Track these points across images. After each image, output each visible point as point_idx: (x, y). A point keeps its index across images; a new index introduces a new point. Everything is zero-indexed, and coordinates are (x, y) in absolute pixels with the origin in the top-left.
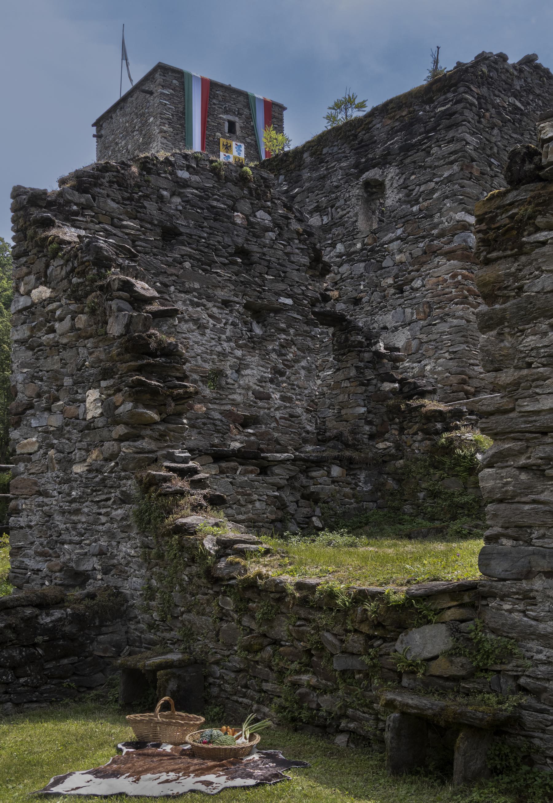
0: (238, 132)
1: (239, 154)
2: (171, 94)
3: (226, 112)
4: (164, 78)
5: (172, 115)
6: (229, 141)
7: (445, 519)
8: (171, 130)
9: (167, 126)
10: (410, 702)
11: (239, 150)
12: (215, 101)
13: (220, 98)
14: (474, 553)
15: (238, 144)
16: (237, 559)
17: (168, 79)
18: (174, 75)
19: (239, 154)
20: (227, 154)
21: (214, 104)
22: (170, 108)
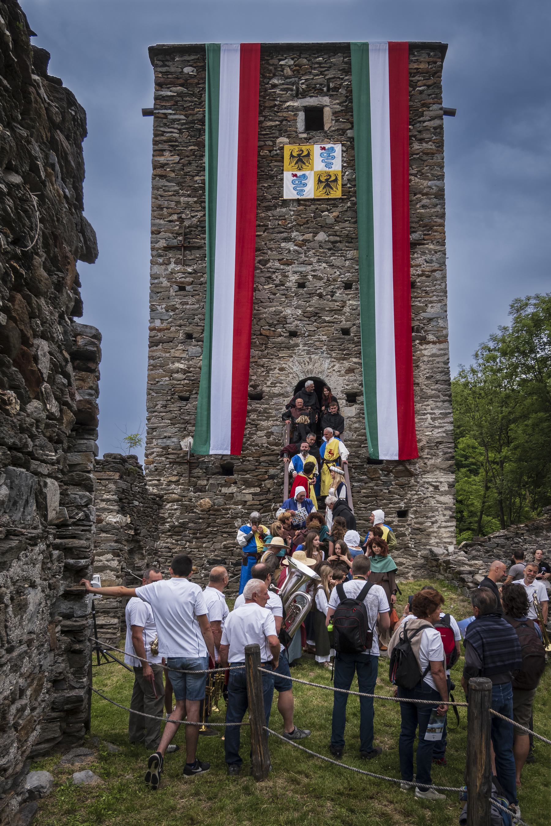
0: (329, 122)
1: (329, 165)
2: (180, 94)
3: (299, 95)
4: (164, 69)
5: (180, 131)
6: (305, 148)
7: (264, 729)
8: (177, 158)
9: (167, 154)
10: (296, 104)
11: (328, 154)
12: (275, 81)
13: (288, 71)
14: (296, 689)
15: (327, 146)
16: (332, 822)
17: (173, 69)
18: (187, 58)
19: (329, 165)
20: (299, 173)
21: (274, 86)
22: (174, 120)
